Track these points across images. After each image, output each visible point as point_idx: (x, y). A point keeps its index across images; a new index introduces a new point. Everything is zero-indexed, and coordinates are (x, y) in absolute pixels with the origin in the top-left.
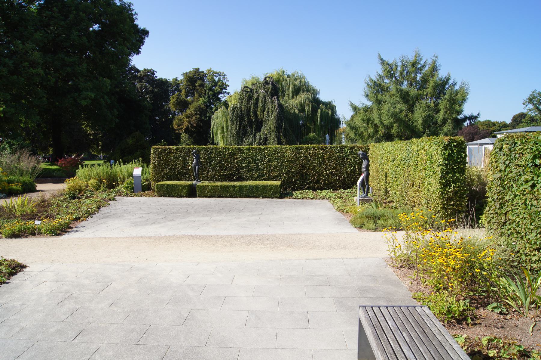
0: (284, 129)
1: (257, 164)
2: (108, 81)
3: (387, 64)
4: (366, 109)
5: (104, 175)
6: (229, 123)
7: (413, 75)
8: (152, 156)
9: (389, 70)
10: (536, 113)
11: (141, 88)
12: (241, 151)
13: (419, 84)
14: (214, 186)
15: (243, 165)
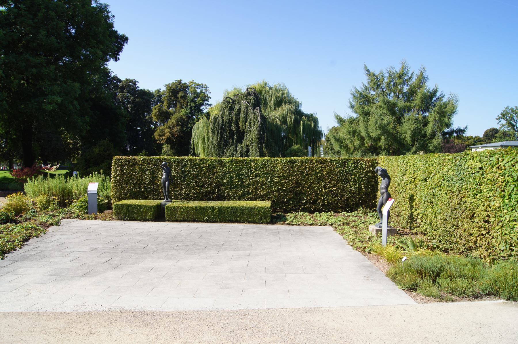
0: (267, 140)
1: (241, 180)
2: (77, 85)
3: (374, 75)
4: (352, 121)
5: (56, 190)
6: (210, 134)
7: (399, 87)
8: (113, 168)
9: (376, 82)
10: (509, 128)
11: (122, 97)
12: (221, 164)
13: (406, 95)
14: (188, 207)
15: (225, 181)
